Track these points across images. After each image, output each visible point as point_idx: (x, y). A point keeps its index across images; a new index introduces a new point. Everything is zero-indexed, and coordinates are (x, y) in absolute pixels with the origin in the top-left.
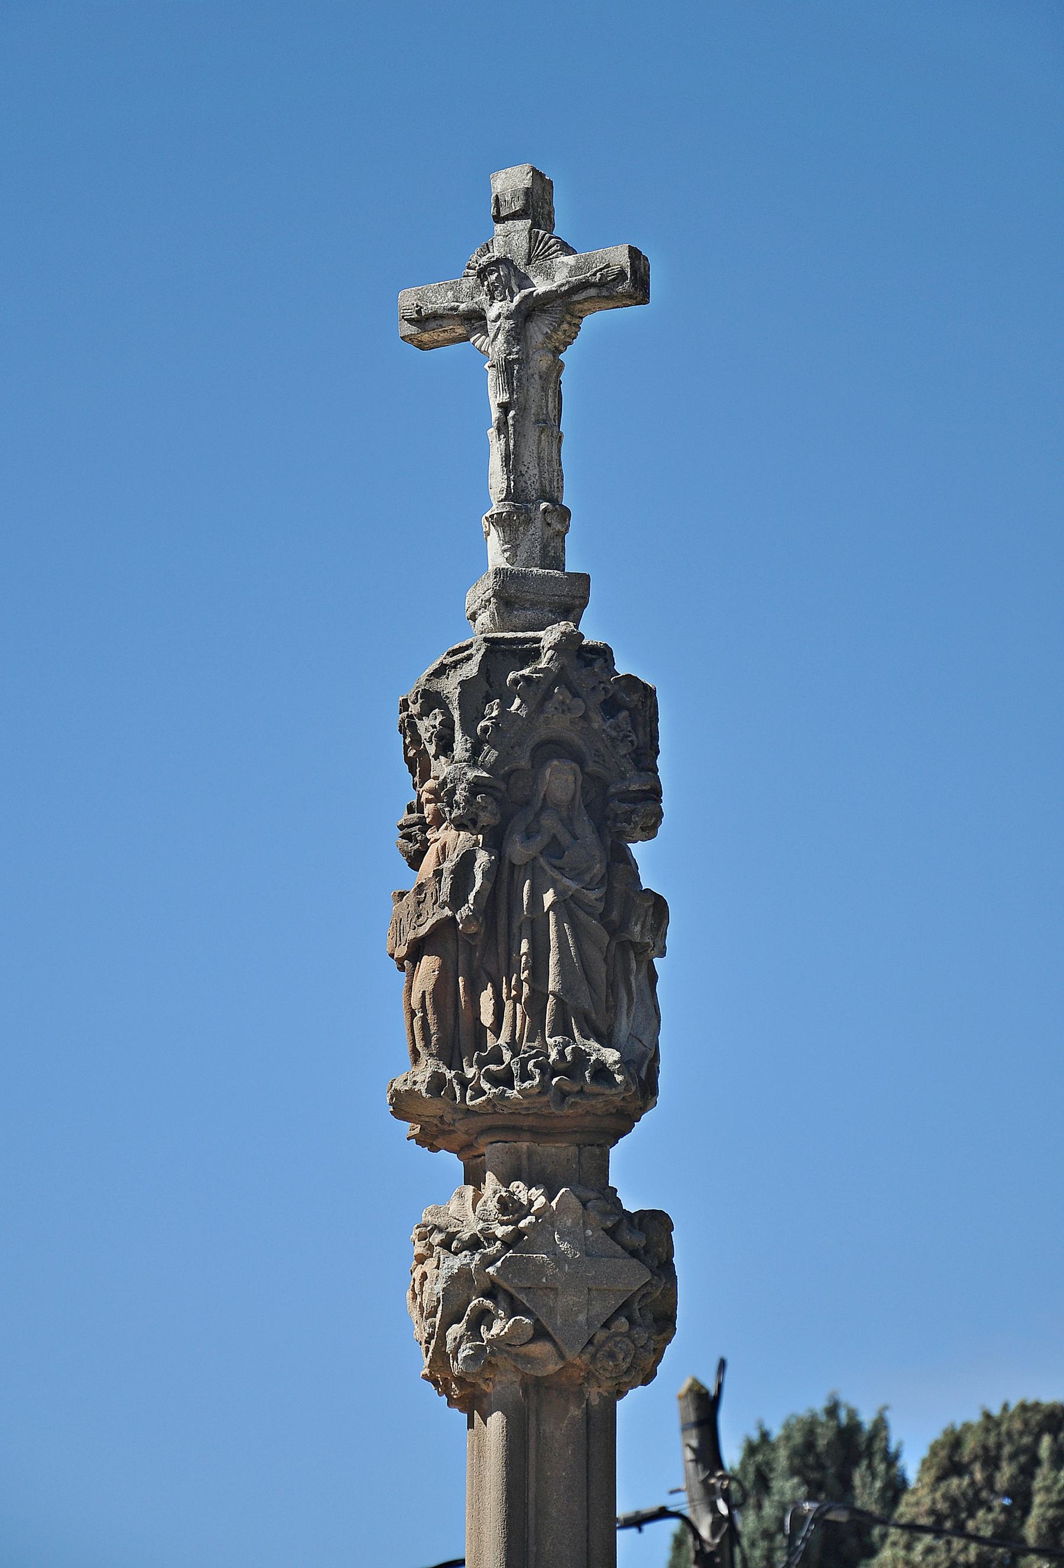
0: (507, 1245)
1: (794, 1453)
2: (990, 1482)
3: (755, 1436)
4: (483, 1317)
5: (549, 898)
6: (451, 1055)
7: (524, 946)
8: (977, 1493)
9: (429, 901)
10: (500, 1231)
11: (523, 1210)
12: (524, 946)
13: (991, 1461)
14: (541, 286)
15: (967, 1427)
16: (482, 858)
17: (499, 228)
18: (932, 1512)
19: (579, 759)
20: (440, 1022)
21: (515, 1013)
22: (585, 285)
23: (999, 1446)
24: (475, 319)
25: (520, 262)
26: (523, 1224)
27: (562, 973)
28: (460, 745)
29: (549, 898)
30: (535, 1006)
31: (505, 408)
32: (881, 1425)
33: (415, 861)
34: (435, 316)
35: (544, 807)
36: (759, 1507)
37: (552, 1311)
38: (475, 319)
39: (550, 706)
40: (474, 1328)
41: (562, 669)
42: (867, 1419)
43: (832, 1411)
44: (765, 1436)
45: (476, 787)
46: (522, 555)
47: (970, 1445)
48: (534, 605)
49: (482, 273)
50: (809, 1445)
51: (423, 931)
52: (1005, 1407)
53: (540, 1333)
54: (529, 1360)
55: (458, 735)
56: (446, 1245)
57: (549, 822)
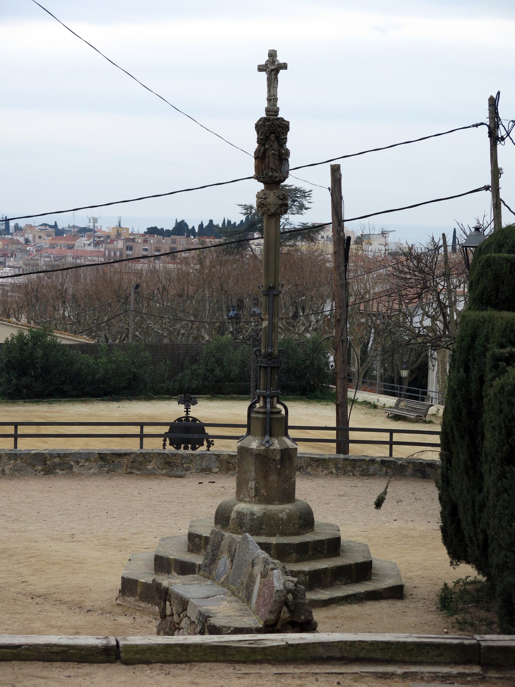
3: (42, 473)
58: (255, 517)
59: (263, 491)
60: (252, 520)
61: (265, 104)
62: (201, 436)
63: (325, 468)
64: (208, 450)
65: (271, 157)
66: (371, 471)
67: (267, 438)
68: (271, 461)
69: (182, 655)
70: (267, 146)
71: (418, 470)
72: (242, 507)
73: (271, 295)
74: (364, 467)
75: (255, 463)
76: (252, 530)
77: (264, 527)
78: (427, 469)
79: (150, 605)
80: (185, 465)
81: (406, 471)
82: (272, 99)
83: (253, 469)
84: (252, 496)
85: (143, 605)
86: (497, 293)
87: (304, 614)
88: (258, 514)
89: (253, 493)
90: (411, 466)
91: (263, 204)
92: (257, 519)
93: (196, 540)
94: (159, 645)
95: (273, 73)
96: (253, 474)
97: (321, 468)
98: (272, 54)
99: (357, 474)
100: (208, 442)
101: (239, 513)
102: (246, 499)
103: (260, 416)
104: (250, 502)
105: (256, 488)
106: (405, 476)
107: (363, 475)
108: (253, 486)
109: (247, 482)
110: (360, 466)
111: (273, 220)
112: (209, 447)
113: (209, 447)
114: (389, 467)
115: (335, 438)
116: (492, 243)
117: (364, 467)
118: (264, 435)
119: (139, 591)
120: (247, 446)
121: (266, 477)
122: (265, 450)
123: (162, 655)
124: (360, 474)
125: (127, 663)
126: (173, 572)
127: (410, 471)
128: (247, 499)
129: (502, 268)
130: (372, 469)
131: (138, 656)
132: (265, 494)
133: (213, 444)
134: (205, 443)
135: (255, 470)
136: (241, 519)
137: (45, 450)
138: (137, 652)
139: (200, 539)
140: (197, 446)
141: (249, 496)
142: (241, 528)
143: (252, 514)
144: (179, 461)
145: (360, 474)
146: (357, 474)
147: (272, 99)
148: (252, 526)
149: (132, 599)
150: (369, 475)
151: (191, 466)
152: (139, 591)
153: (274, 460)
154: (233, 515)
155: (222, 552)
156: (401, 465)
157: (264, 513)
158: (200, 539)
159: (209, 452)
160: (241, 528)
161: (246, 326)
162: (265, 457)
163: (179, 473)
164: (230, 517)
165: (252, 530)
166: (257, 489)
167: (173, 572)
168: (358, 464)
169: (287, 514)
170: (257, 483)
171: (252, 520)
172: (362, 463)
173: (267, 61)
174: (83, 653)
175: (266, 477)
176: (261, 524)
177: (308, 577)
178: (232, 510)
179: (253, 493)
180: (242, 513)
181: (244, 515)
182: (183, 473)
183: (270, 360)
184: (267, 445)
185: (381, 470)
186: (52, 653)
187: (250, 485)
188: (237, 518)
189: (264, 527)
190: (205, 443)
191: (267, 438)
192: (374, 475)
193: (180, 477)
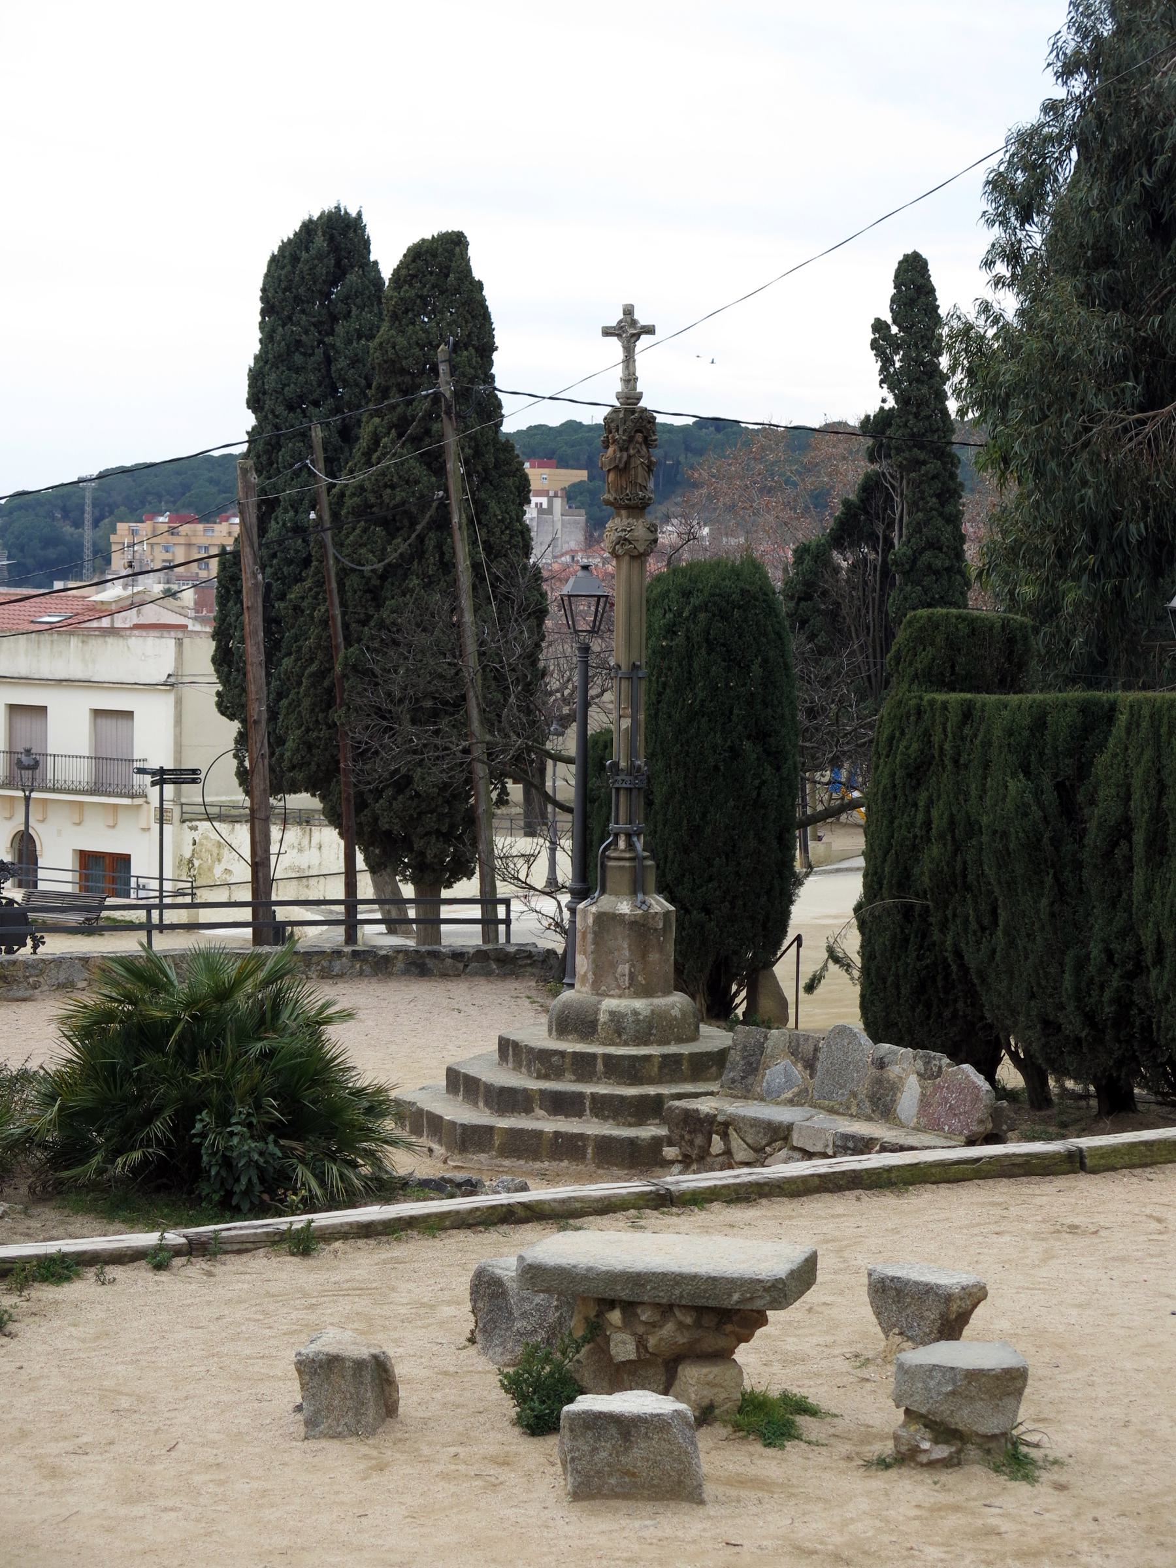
32: (359, 214)
58: (641, 1017)
59: (640, 978)
60: (637, 1022)
61: (619, 387)
62: (24, 929)
64: (35, 953)
65: (640, 468)
66: (336, 970)
67: (640, 897)
69: (1146, 1156)
70: (632, 452)
71: (413, 963)
72: (610, 1004)
73: (635, 679)
74: (325, 963)
75: (629, 935)
76: (637, 1038)
77: (654, 1031)
78: (427, 961)
79: (522, 1162)
80: (31, 980)
81: (394, 965)
82: (630, 379)
83: (626, 946)
85: (507, 1162)
86: (953, 667)
87: (1006, 1123)
88: (645, 1013)
90: (401, 956)
91: (626, 539)
92: (644, 1021)
93: (555, 1059)
94: (1123, 1144)
95: (633, 340)
96: (627, 953)
98: (629, 311)
99: (314, 976)
100: (34, 939)
101: (612, 1013)
103: (627, 864)
104: (620, 997)
105: (631, 973)
106: (391, 974)
107: (323, 978)
108: (627, 972)
109: (613, 965)
110: (318, 963)
111: (636, 564)
112: (35, 947)
113: (35, 947)
114: (365, 961)
115: (250, 919)
116: (669, 591)
117: (325, 963)
118: (634, 893)
119: (497, 1143)
121: (644, 956)
122: (642, 915)
123: (1126, 1158)
124: (318, 976)
125: (1094, 1171)
127: (400, 964)
128: (617, 991)
129: (957, 629)
130: (337, 966)
131: (1103, 1162)
133: (43, 943)
134: (29, 941)
135: (630, 946)
136: (619, 1021)
138: (1102, 1157)
140: (16, 948)
141: (619, 987)
142: (620, 1036)
143: (635, 1013)
144: (20, 974)
145: (318, 976)
146: (314, 976)
147: (630, 379)
148: (638, 1031)
149: (483, 1157)
150: (332, 977)
151: (41, 980)
152: (497, 1143)
153: (656, 930)
154: (603, 1017)
155: (772, 1057)
156: (384, 956)
157: (653, 1011)
159: (34, 957)
160: (620, 1036)
162: (644, 925)
163: (21, 994)
164: (597, 1020)
165: (637, 1038)
166: (632, 976)
168: (315, 959)
169: (681, 1010)
170: (633, 965)
171: (637, 1022)
172: (321, 957)
173: (621, 321)
174: (1046, 1162)
175: (644, 956)
176: (650, 1027)
178: (598, 1009)
180: (619, 1012)
181: (624, 1016)
182: (30, 992)
183: (636, 778)
184: (644, 907)
185: (352, 967)
186: (1014, 1165)
187: (619, 970)
188: (612, 1021)
189: (654, 1031)
190: (29, 941)
191: (640, 897)
192: (341, 976)
193: (24, 1000)
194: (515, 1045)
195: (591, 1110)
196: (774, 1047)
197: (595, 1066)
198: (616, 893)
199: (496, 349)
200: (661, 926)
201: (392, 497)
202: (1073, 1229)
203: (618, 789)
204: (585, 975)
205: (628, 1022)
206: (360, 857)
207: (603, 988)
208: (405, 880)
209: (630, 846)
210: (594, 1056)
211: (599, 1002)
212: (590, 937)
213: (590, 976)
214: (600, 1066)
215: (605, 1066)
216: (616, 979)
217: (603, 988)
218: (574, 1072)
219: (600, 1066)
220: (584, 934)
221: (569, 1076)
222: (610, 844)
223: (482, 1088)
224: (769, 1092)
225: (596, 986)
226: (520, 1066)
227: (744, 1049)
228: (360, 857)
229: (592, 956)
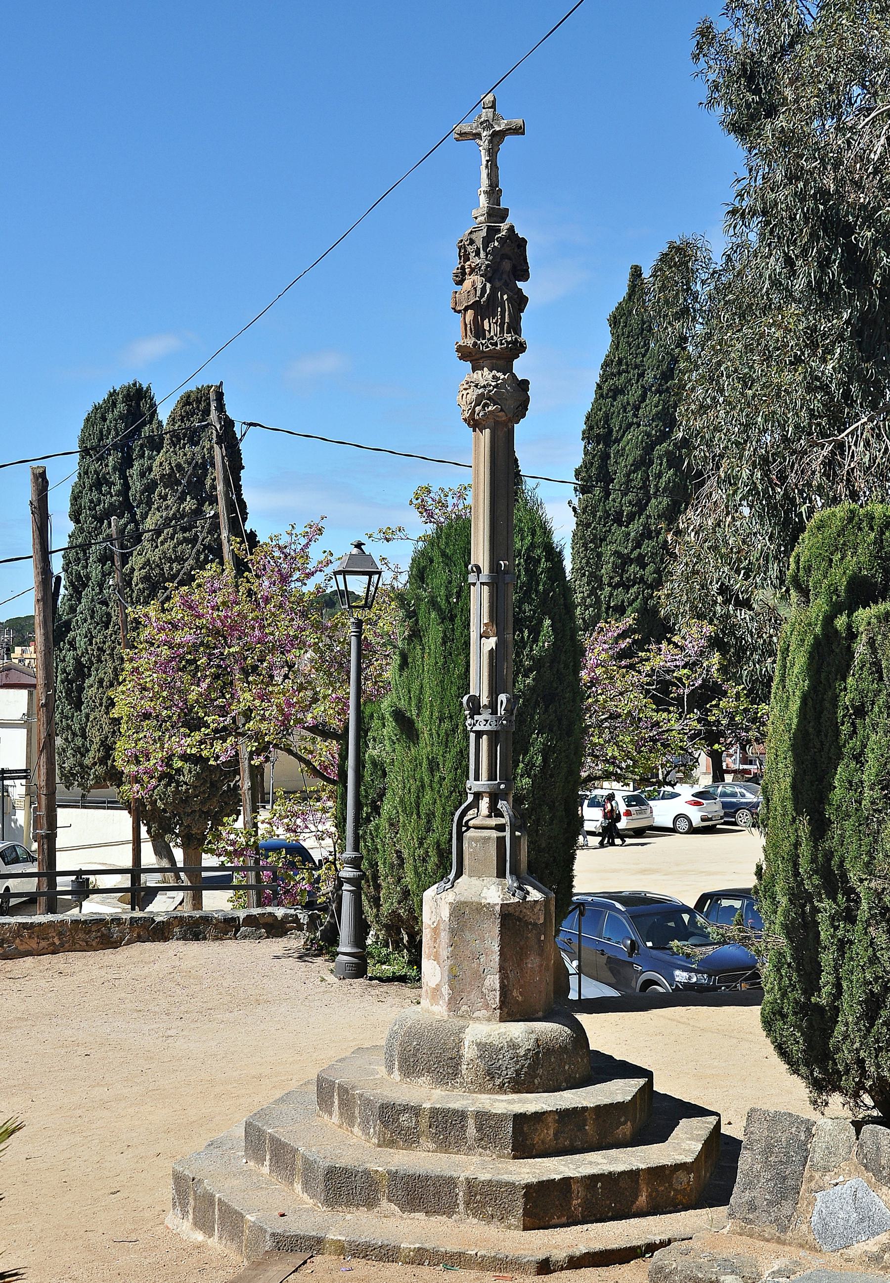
0: (494, 387)
1: (124, 396)
2: (198, 407)
3: (112, 391)
4: (486, 405)
5: (505, 297)
6: (477, 337)
7: (499, 309)
8: (194, 410)
9: (472, 296)
10: (493, 384)
11: (498, 379)
12: (499, 309)
13: (199, 402)
14: (498, 129)
15: (191, 392)
16: (488, 285)
17: (484, 110)
18: (181, 415)
19: (510, 259)
20: (474, 328)
21: (497, 329)
22: (510, 129)
23: (201, 397)
24: (478, 136)
25: (491, 121)
26: (499, 382)
27: (510, 317)
28: (482, 254)
29: (505, 297)
30: (502, 326)
31: (488, 161)
32: (149, 388)
33: (460, 283)
34: (465, 133)
35: (502, 273)
36: (113, 411)
37: (505, 405)
38: (478, 136)
39: (505, 245)
40: (483, 407)
41: (509, 235)
42: (145, 387)
43: (135, 384)
44: (115, 391)
45: (487, 266)
46: (491, 201)
47: (193, 396)
48: (496, 216)
49: (482, 123)
50: (128, 395)
51: (470, 303)
52: (203, 386)
53: (502, 410)
54: (498, 416)
55: (482, 251)
56: (476, 386)
57: (505, 276)
63: (43, 939)
68: (530, 927)
84: (494, 1006)
89: (498, 1000)
97: (36, 939)
101: (483, 1047)
102: (477, 1014)
104: (489, 1020)
120: (476, 899)
126: (384, 1203)
132: (520, 999)
137: (217, 911)
139: (417, 1115)
143: (513, 1046)
153: (535, 924)
154: (469, 1052)
158: (417, 1115)
161: (844, 287)
167: (384, 1203)
171: (515, 1058)
177: (692, 1175)
178: (461, 1040)
179: (495, 999)
180: (491, 1045)
187: (487, 983)
194: (344, 1091)
195: (467, 1204)
196: (830, 1151)
197: (463, 1128)
198: (477, 874)
199: (243, 468)
200: (541, 921)
201: (171, 569)
202: (837, 1184)
203: (479, 734)
204: (437, 989)
205: (505, 1060)
206: (144, 829)
207: (464, 1008)
208: (177, 845)
209: (494, 811)
210: (462, 1115)
211: (462, 1029)
212: (444, 937)
213: (445, 990)
214: (471, 1130)
215: (479, 1129)
216: (483, 995)
217: (464, 1008)
218: (434, 1137)
219: (471, 1130)
220: (436, 930)
221: (427, 1143)
222: (469, 808)
223: (299, 1163)
224: (825, 1232)
225: (454, 1003)
226: (351, 1124)
227: (768, 1150)
228: (144, 829)
229: (449, 963)
